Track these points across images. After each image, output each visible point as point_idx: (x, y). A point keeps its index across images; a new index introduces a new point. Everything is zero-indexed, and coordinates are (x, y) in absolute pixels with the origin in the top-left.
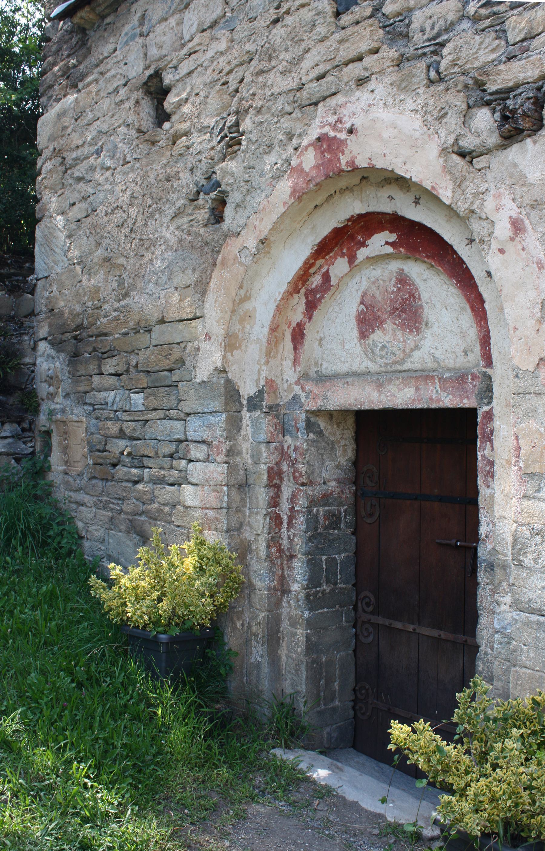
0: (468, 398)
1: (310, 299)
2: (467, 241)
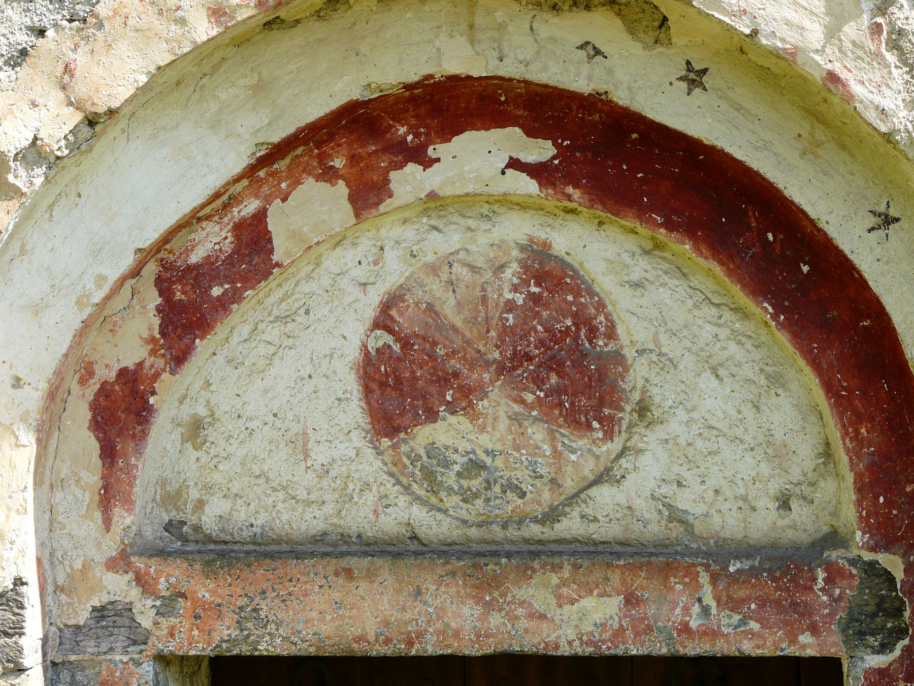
0: (814, 630)
2: (872, 221)
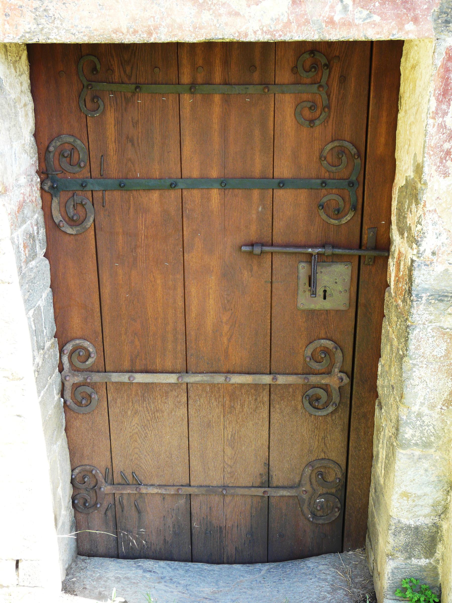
0: (415, 20)
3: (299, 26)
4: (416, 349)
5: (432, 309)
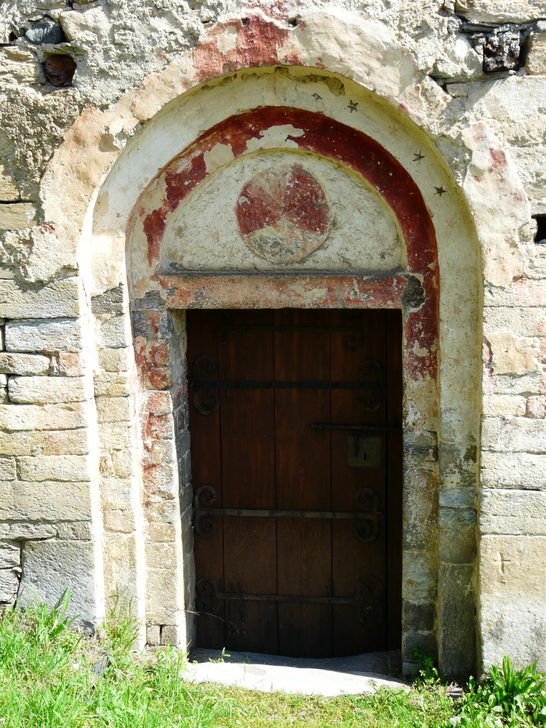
0: (392, 300)
1: (173, 185)
3: (332, 301)
4: (409, 483)
5: (416, 457)
